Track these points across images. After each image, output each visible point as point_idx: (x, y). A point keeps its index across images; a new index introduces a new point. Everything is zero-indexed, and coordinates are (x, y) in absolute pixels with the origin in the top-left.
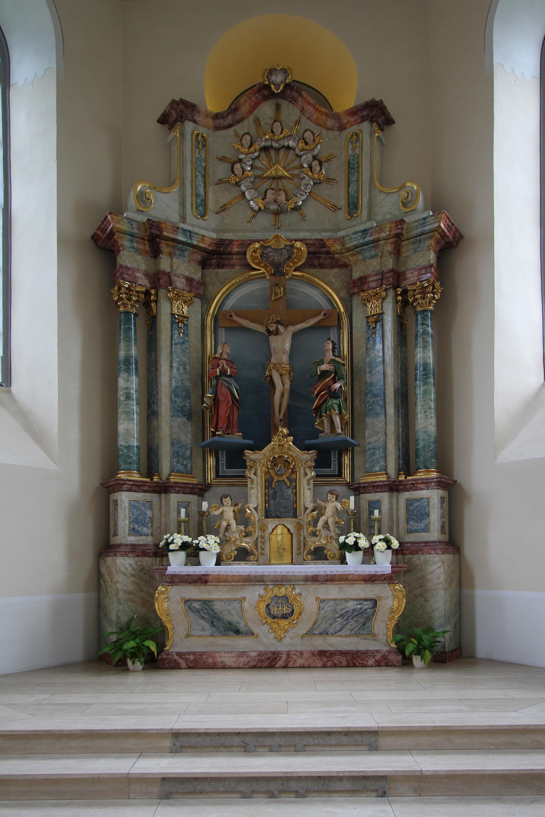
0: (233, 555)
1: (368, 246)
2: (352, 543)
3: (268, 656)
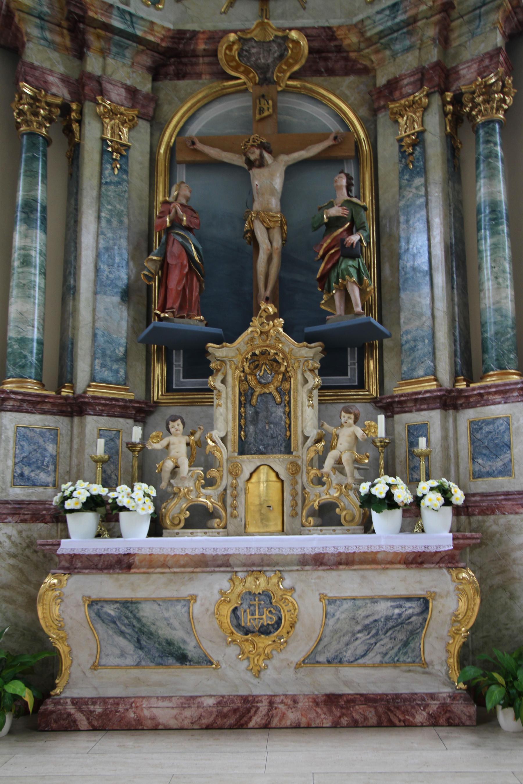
0: (182, 518)
1: (400, 32)
2: (383, 495)
3: (235, 707)
